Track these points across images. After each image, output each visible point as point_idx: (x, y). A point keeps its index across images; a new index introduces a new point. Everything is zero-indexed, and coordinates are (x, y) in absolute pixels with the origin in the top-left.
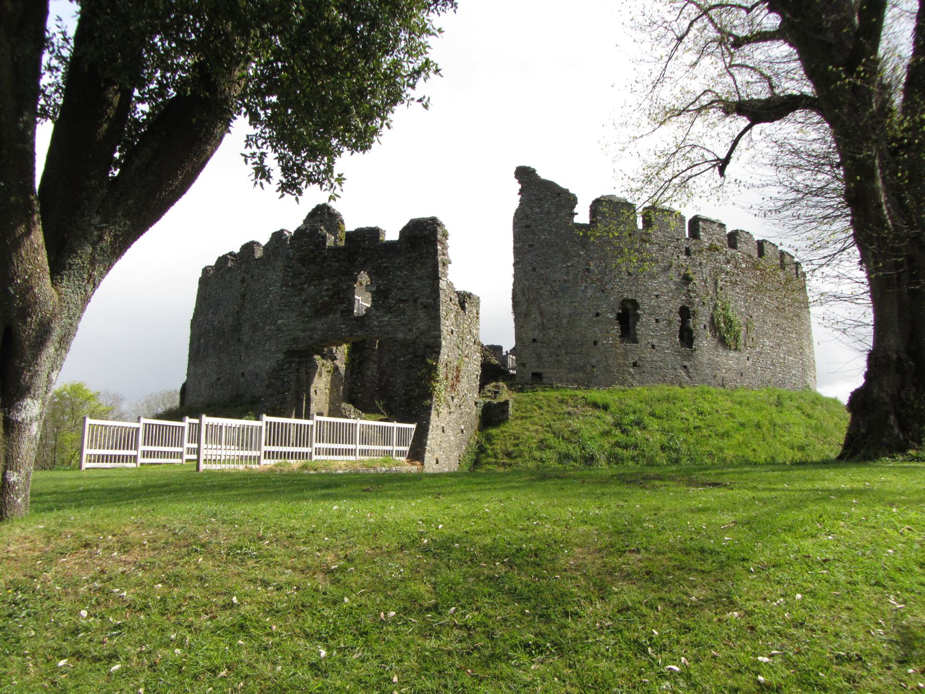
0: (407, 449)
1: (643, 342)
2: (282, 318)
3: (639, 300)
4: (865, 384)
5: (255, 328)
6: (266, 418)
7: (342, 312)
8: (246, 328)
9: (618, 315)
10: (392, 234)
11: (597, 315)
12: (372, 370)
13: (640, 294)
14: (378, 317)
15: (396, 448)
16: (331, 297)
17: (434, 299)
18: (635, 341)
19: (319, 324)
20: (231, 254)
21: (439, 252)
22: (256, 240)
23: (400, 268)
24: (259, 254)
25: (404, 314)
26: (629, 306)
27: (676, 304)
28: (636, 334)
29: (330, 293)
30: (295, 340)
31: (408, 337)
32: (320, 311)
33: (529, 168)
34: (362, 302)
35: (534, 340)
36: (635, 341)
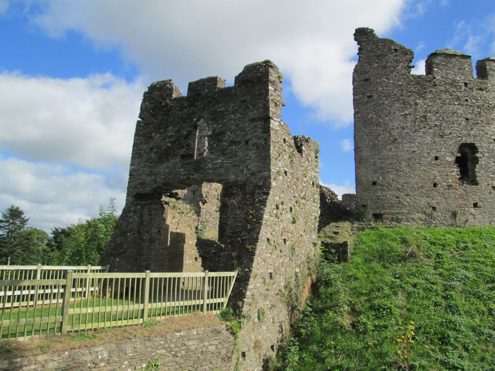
1: (483, 184)
3: (477, 145)
7: (183, 157)
10: (228, 79)
13: (478, 138)
15: (208, 301)
16: (173, 143)
17: (265, 139)
18: (474, 182)
19: (163, 168)
21: (270, 93)
25: (236, 156)
26: (467, 150)
28: (476, 177)
29: (173, 139)
31: (239, 179)
33: (367, 29)
35: (374, 183)
36: (474, 182)
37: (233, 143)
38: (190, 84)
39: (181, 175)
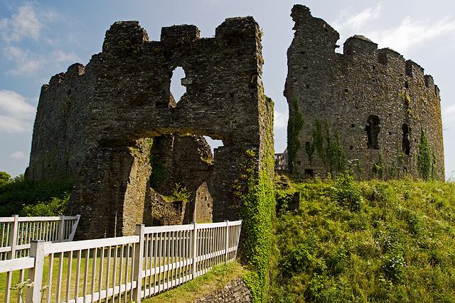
0: (235, 248)
2: (96, 108)
5: (77, 127)
8: (71, 127)
9: (367, 126)
10: (207, 31)
11: (353, 126)
12: (169, 163)
14: (194, 109)
15: (197, 259)
17: (252, 94)
19: (134, 114)
20: (61, 74)
23: (217, 64)
24: (81, 73)
25: (222, 108)
27: (401, 122)
32: (140, 101)
34: (177, 90)
37: (216, 95)
38: (163, 28)
39: (158, 123)
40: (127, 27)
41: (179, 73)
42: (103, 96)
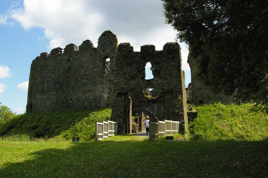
2: (116, 80)
4: (25, 114)
6: (166, 121)
7: (141, 78)
10: (159, 48)
14: (156, 80)
17: (179, 74)
22: (73, 43)
30: (122, 88)
32: (134, 78)
34: (149, 75)
35: (200, 88)
40: (126, 46)
41: (148, 65)
42: (118, 75)
